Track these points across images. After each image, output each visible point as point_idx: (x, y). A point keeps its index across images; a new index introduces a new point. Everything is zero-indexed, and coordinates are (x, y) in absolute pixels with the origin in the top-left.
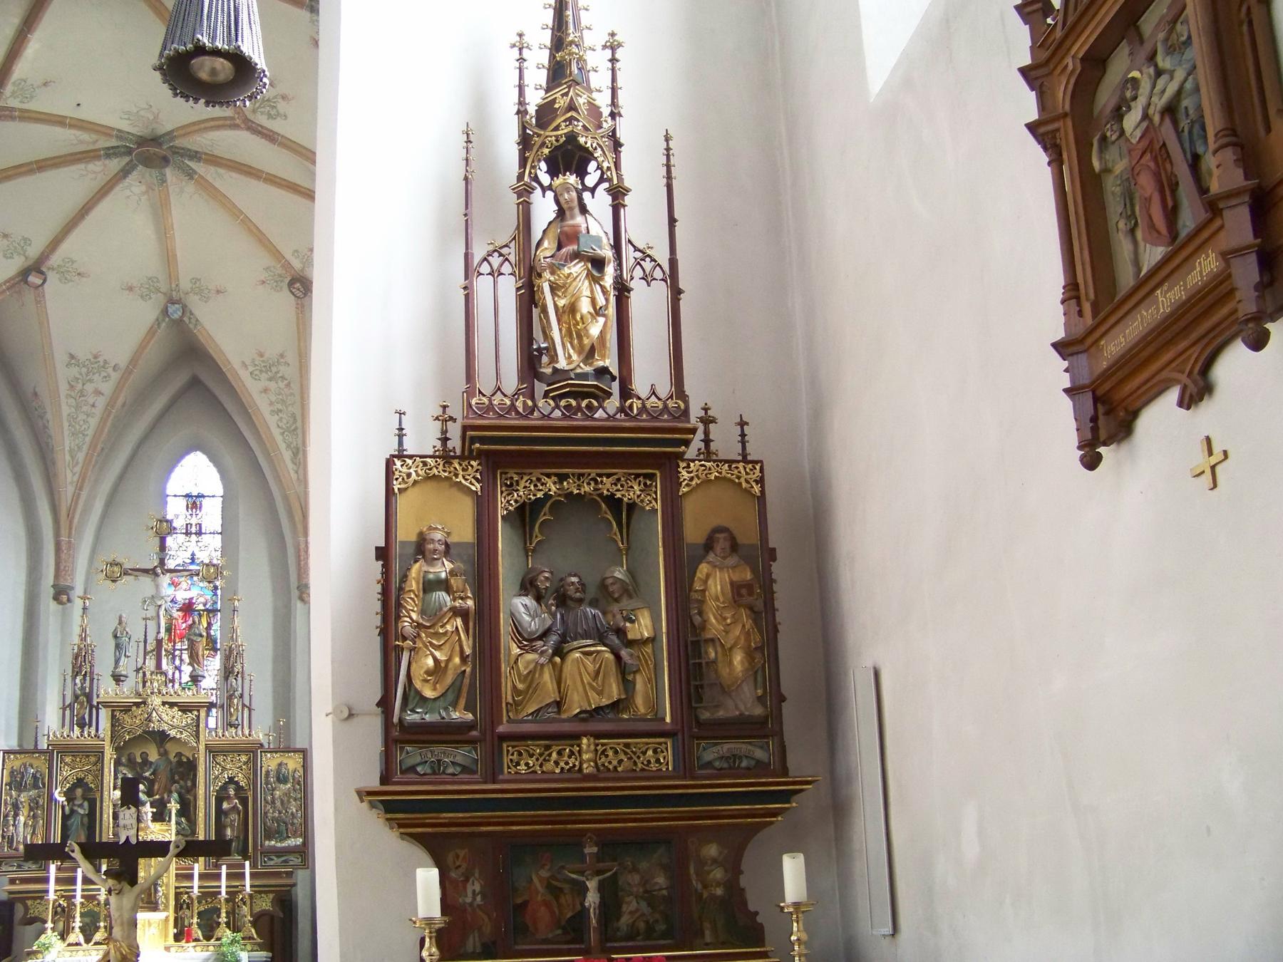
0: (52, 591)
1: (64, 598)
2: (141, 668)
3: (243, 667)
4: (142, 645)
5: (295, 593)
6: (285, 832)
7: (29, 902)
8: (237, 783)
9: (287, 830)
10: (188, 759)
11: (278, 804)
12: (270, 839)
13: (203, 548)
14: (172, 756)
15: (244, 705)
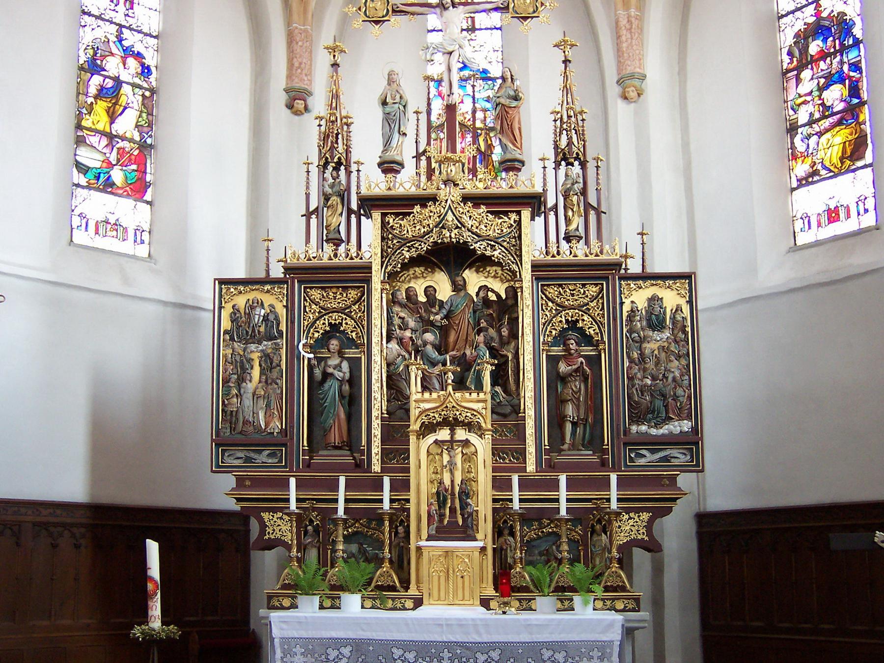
0: (283, 98)
1: (299, 104)
2: (425, 151)
3: (584, 146)
4: (423, 117)
5: (613, 90)
6: (663, 409)
7: (266, 516)
8: (581, 331)
9: (666, 406)
10: (498, 296)
11: (650, 365)
12: (638, 422)
13: (477, 48)
14: (472, 290)
15: (588, 206)
